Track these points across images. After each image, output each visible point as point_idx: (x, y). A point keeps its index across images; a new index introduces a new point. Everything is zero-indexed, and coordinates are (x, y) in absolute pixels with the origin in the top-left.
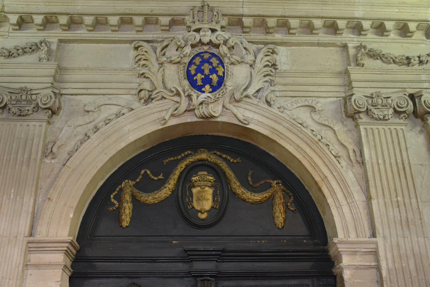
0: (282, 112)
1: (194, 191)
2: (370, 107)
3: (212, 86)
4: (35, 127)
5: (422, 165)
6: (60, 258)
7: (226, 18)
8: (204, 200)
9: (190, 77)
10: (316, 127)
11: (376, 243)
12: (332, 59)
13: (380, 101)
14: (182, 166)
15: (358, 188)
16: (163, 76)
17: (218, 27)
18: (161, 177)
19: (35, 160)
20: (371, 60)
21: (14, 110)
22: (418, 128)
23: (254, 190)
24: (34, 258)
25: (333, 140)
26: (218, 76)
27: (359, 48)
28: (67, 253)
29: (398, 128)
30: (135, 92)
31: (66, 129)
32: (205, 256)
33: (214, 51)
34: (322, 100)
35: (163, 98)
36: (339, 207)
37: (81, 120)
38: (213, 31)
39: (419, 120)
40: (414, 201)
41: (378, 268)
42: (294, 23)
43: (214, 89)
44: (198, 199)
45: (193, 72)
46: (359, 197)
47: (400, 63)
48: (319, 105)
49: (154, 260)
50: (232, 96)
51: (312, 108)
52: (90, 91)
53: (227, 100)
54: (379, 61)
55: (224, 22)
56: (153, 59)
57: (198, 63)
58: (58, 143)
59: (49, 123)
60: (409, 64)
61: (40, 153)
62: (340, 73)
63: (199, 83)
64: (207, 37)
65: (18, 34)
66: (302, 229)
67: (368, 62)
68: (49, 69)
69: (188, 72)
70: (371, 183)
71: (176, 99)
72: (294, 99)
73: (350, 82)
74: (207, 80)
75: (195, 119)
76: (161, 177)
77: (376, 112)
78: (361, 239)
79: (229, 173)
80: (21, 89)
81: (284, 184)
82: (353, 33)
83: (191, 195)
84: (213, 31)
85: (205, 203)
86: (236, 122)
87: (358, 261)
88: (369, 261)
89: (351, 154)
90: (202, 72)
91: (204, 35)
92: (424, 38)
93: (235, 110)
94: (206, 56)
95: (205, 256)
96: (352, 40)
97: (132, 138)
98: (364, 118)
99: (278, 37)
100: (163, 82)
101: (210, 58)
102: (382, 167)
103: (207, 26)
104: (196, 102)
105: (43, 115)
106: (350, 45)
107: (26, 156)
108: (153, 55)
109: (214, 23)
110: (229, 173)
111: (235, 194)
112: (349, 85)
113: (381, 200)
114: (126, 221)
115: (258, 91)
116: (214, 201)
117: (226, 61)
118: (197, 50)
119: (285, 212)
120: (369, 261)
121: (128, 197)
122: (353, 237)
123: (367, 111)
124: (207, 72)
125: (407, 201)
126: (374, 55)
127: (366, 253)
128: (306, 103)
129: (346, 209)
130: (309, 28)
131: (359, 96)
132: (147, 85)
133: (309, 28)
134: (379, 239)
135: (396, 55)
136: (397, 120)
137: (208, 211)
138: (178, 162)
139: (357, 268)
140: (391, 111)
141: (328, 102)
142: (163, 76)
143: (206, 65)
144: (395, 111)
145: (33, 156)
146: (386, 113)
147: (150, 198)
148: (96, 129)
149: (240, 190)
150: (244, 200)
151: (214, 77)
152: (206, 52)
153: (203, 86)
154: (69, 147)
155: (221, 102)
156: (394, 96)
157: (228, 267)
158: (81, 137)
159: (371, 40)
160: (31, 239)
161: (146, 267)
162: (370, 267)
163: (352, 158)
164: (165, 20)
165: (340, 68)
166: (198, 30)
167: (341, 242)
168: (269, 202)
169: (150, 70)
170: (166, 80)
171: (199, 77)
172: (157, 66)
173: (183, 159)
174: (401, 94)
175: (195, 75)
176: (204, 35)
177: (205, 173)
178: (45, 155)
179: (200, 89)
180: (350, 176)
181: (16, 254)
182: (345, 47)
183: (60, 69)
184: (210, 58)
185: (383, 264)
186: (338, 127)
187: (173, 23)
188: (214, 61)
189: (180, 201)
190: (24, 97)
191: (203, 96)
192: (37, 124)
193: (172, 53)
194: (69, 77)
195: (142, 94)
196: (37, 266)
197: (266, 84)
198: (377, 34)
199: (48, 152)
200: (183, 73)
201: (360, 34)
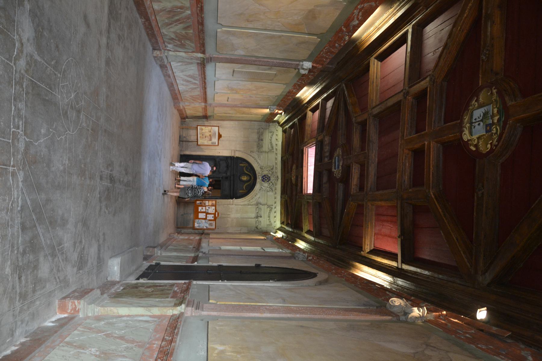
4: (255, 149)
6: (233, 155)
8: (245, 178)
9: (265, 176)
23: (246, 187)
46: (242, 204)
67: (269, 209)
68: (267, 150)
114: (241, 165)
130: (275, 198)
133: (275, 198)
141: (262, 201)
147: (244, 169)
157: (232, 182)
159: (273, 210)
168: (243, 190)
180: (246, 203)
181: (233, 148)
193: (270, 172)
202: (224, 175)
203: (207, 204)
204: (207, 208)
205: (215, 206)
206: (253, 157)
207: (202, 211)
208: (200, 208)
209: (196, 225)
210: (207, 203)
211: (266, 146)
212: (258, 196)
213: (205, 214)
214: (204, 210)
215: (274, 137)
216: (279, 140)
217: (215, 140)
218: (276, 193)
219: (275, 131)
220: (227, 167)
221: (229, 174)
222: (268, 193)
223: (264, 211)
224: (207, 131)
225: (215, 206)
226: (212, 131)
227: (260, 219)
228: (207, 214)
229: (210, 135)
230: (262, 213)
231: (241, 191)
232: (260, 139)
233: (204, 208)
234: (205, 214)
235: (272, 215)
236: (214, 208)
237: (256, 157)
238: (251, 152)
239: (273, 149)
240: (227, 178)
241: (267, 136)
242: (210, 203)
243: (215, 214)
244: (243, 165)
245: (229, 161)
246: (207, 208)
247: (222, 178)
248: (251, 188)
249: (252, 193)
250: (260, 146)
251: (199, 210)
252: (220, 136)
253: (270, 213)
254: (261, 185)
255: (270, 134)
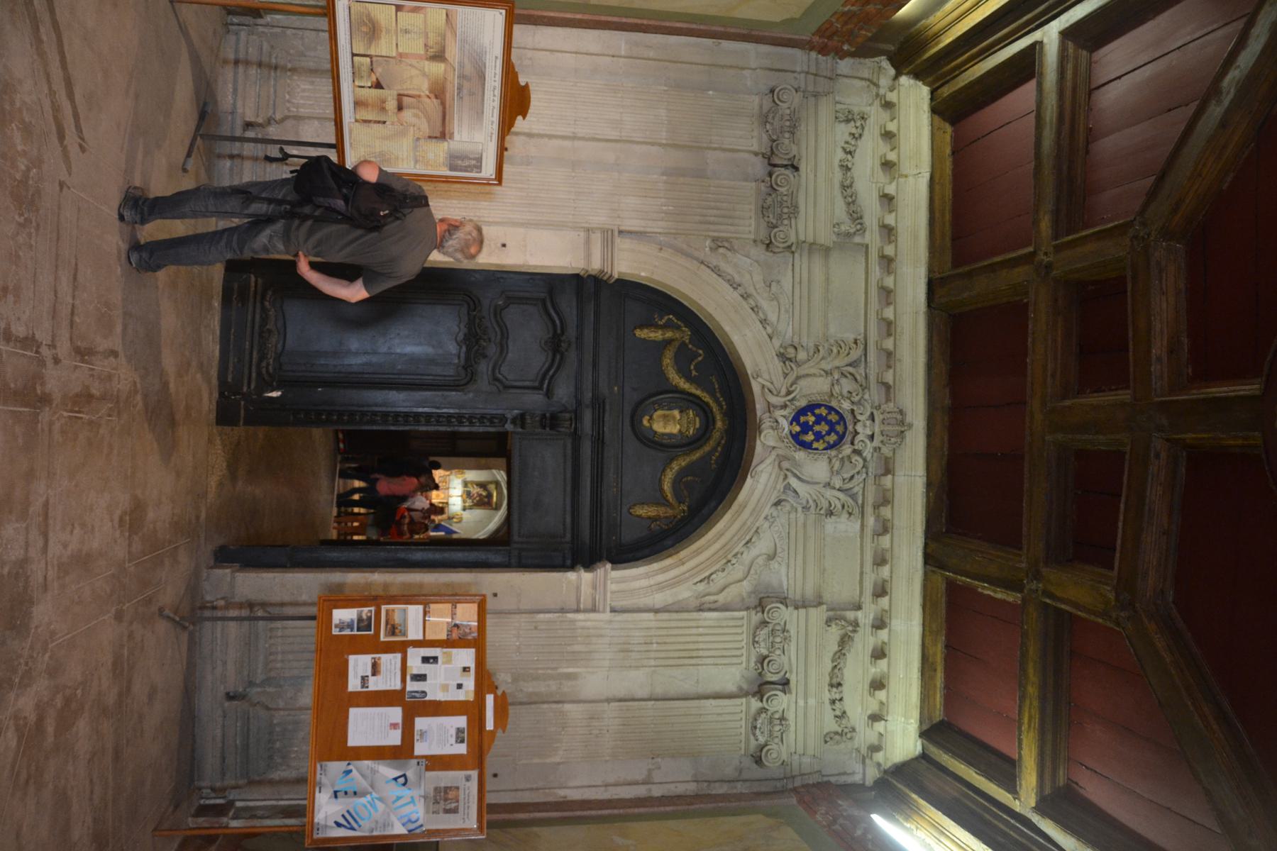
0: (766, 518)
1: (676, 413)
2: (771, 626)
3: (798, 434)
4: (748, 225)
5: (698, 682)
6: (596, 265)
7: (891, 454)
9: (811, 408)
10: (747, 557)
11: (604, 612)
12: (841, 587)
13: (778, 640)
14: (706, 398)
15: (670, 601)
16: (814, 375)
17: (876, 443)
18: (694, 373)
19: (708, 230)
20: (838, 639)
21: (769, 200)
22: (745, 686)
23: (676, 483)
24: (597, 239)
25: (730, 579)
26: (811, 443)
27: (856, 624)
28: (602, 271)
29: (744, 659)
30: (796, 339)
31: (747, 265)
32: (598, 421)
33: (848, 438)
34: (783, 570)
35: (786, 375)
36: (647, 576)
37: (758, 278)
38: (872, 437)
39: (756, 689)
40: (653, 663)
41: (578, 611)
42: (885, 541)
43: (795, 437)
44: (665, 416)
45: (817, 411)
46: (659, 599)
47: (832, 675)
48: (776, 566)
49: (595, 365)
50: (786, 458)
51: (772, 557)
52: (797, 286)
53: (780, 452)
54: (836, 648)
55: (886, 451)
56: (837, 363)
57: (830, 417)
58: (729, 254)
59: (755, 241)
60: (832, 685)
61: (716, 234)
62: (820, 597)
63: (802, 419)
64: (863, 430)
65: (875, 195)
66: (628, 535)
67: (835, 632)
68: (825, 236)
69: (819, 406)
70: (675, 616)
71: (784, 391)
72: (784, 534)
73: (804, 607)
74: (806, 428)
75: (759, 413)
76: (694, 373)
77: (763, 633)
78: (609, 595)
79: (696, 456)
80: (796, 207)
81: (683, 519)
82: (875, 619)
83: (670, 409)
84: (872, 437)
85: (661, 424)
86: (754, 464)
87: (586, 590)
88: (585, 601)
89: (712, 598)
90: (817, 422)
91: (865, 426)
92: (869, 712)
93: (768, 461)
94: (839, 428)
95: (598, 421)
96: (865, 617)
97: (736, 339)
98: (756, 617)
99: (871, 521)
100: (808, 375)
101: (837, 433)
102: (694, 631)
103: (877, 430)
104: (778, 413)
105: (763, 234)
106: (860, 614)
107: (712, 219)
108: (843, 363)
109: (881, 438)
110: (696, 456)
111: (672, 460)
112: (801, 605)
113: (653, 624)
114: (642, 334)
115: (795, 491)
116: (663, 434)
117: (833, 453)
118: (848, 417)
119: (649, 518)
120: (585, 601)
121: (669, 334)
122: (612, 587)
123: (764, 623)
124: (817, 428)
125: (653, 655)
126: (844, 641)
127: (594, 599)
128: (779, 550)
129: (644, 583)
130: (880, 561)
131: (785, 614)
132: (802, 355)
133: (880, 561)
134: (607, 616)
135: (846, 671)
136: (753, 659)
137: (651, 428)
138: (713, 395)
139: (578, 588)
140: (765, 652)
141: (782, 576)
142: (814, 375)
143: (827, 428)
144: (765, 658)
145: (712, 227)
146: (762, 644)
147: (668, 360)
148: (746, 297)
149: (676, 466)
150: (664, 470)
151: (810, 437)
152: (846, 428)
153: (798, 424)
154: (723, 266)
155: (779, 444)
156: (785, 659)
158: (737, 279)
159: (865, 641)
160: (616, 233)
161: (588, 357)
162: (578, 602)
163: (707, 598)
164: (889, 377)
165: (827, 597)
166: (872, 417)
167: (606, 571)
168: (661, 501)
169: (823, 358)
170: (809, 379)
171: (812, 419)
172: (828, 367)
173: (717, 401)
174: (786, 668)
175: (814, 414)
176: (865, 426)
177: (698, 425)
178: (714, 240)
179: (796, 419)
180: (685, 593)
181: (600, 218)
182: (859, 608)
183: (826, 251)
184: (837, 433)
185: (580, 616)
186: (746, 586)
187: (887, 387)
188: (832, 438)
189: (664, 394)
190: (786, 210)
191: (784, 423)
192: (752, 228)
193: (847, 385)
194: (818, 261)
195: (791, 350)
196: (588, 242)
197: (804, 502)
198: (874, 650)
199: (718, 244)
200: (816, 399)
201: (873, 626)
202: (534, 401)
203: (414, 633)
204: (415, 656)
205: (478, 642)
206: (735, 286)
207: (375, 684)
208: (358, 665)
209: (326, 811)
210: (413, 619)
211: (818, 213)
212: (762, 546)
213: (396, 714)
214: (388, 680)
215: (870, 150)
216: (906, 167)
217: (476, 135)
218: (885, 528)
219: (877, 116)
220: (555, 345)
221: (563, 392)
222: (830, 525)
223: (806, 644)
224: (414, 45)
225: (478, 642)
226: (453, 53)
227: (780, 702)
228: (416, 707)
229: (438, 92)
230: (789, 660)
231: (642, 511)
232: (778, 163)
233: (390, 661)
234: (396, 714)
235: (857, 670)
236: (466, 657)
237: (752, 277)
238: (718, 244)
239: (862, 230)
240: (551, 421)
241: (822, 143)
242: (441, 619)
243: (473, 710)
244: (656, 335)
245: (568, 305)
246: (415, 665)
247: (521, 420)
248: (713, 483)
249: (724, 529)
250: (776, 208)
251: (354, 685)
252: (516, 101)
253: (840, 654)
254: (786, 469)
255: (843, 131)
